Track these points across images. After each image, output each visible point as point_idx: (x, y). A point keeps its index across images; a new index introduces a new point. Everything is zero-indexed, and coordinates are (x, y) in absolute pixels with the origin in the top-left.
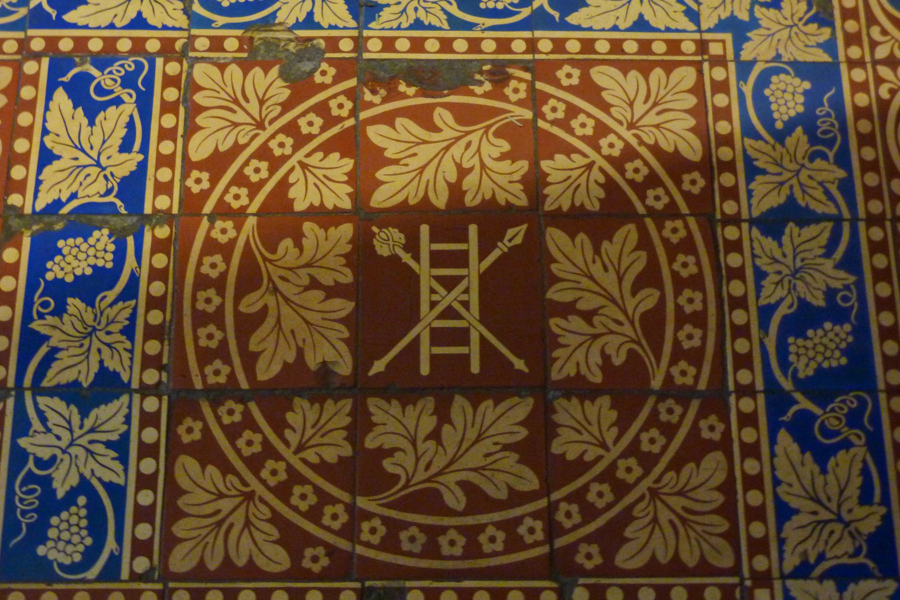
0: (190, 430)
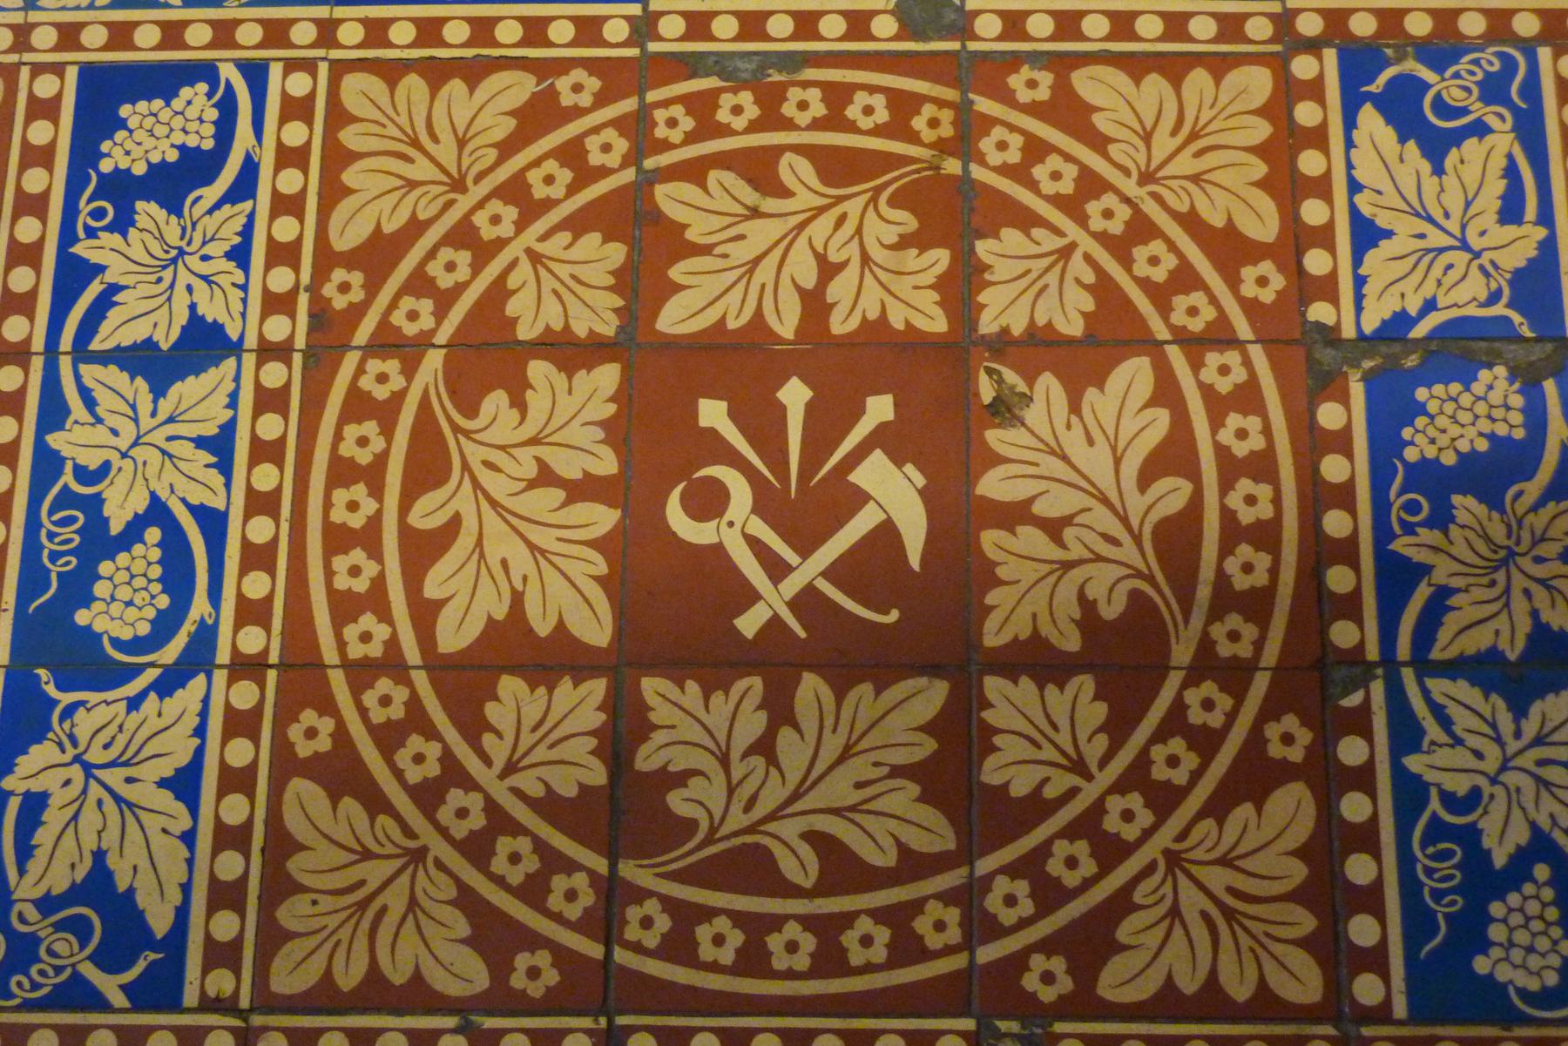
0: (311, 733)
